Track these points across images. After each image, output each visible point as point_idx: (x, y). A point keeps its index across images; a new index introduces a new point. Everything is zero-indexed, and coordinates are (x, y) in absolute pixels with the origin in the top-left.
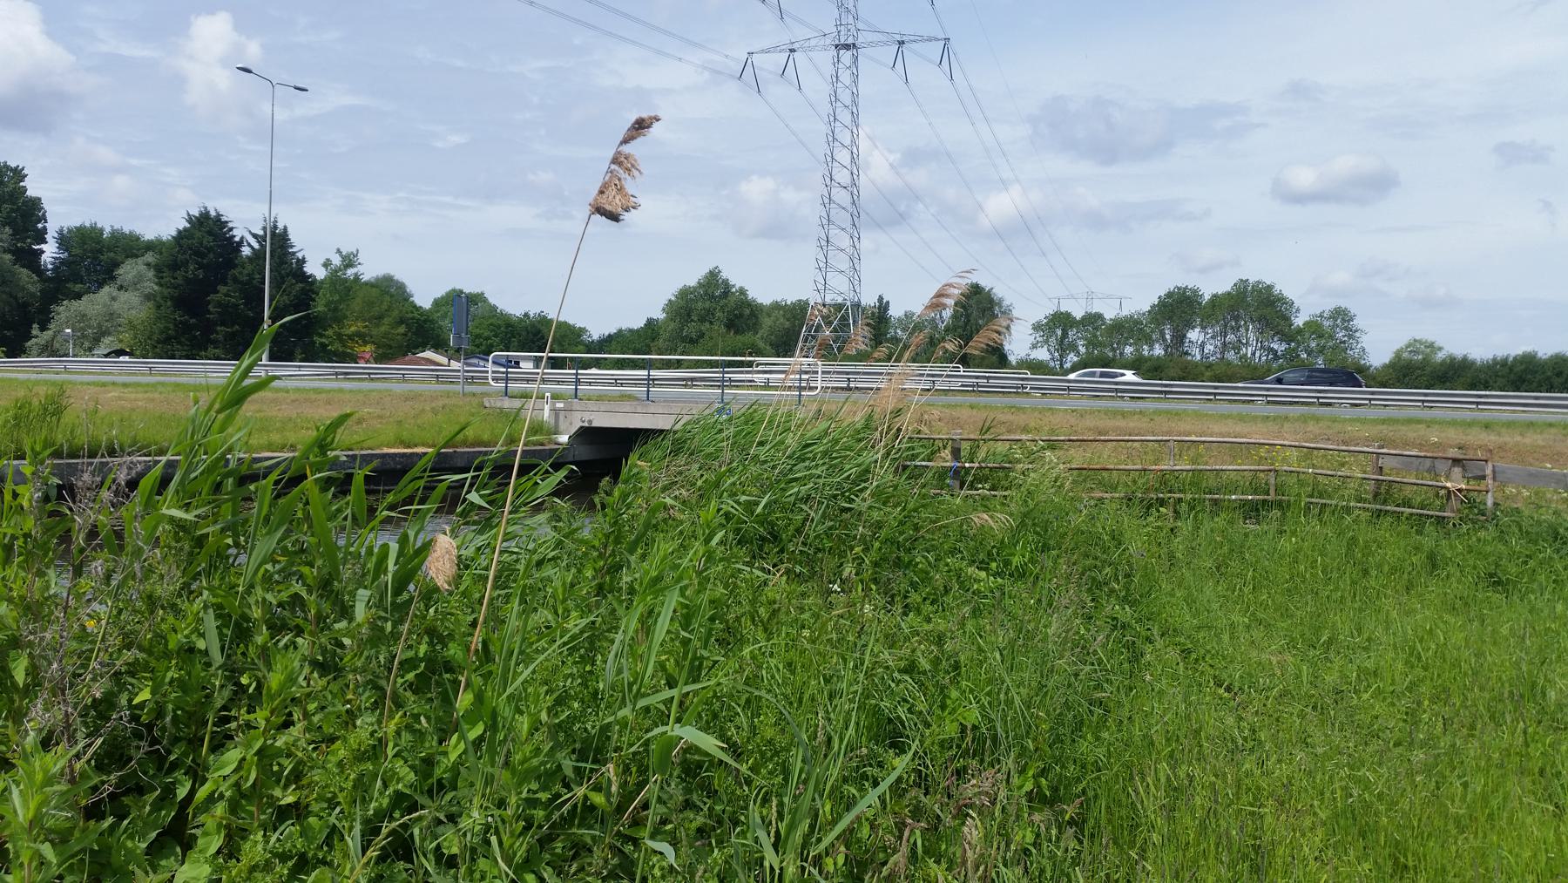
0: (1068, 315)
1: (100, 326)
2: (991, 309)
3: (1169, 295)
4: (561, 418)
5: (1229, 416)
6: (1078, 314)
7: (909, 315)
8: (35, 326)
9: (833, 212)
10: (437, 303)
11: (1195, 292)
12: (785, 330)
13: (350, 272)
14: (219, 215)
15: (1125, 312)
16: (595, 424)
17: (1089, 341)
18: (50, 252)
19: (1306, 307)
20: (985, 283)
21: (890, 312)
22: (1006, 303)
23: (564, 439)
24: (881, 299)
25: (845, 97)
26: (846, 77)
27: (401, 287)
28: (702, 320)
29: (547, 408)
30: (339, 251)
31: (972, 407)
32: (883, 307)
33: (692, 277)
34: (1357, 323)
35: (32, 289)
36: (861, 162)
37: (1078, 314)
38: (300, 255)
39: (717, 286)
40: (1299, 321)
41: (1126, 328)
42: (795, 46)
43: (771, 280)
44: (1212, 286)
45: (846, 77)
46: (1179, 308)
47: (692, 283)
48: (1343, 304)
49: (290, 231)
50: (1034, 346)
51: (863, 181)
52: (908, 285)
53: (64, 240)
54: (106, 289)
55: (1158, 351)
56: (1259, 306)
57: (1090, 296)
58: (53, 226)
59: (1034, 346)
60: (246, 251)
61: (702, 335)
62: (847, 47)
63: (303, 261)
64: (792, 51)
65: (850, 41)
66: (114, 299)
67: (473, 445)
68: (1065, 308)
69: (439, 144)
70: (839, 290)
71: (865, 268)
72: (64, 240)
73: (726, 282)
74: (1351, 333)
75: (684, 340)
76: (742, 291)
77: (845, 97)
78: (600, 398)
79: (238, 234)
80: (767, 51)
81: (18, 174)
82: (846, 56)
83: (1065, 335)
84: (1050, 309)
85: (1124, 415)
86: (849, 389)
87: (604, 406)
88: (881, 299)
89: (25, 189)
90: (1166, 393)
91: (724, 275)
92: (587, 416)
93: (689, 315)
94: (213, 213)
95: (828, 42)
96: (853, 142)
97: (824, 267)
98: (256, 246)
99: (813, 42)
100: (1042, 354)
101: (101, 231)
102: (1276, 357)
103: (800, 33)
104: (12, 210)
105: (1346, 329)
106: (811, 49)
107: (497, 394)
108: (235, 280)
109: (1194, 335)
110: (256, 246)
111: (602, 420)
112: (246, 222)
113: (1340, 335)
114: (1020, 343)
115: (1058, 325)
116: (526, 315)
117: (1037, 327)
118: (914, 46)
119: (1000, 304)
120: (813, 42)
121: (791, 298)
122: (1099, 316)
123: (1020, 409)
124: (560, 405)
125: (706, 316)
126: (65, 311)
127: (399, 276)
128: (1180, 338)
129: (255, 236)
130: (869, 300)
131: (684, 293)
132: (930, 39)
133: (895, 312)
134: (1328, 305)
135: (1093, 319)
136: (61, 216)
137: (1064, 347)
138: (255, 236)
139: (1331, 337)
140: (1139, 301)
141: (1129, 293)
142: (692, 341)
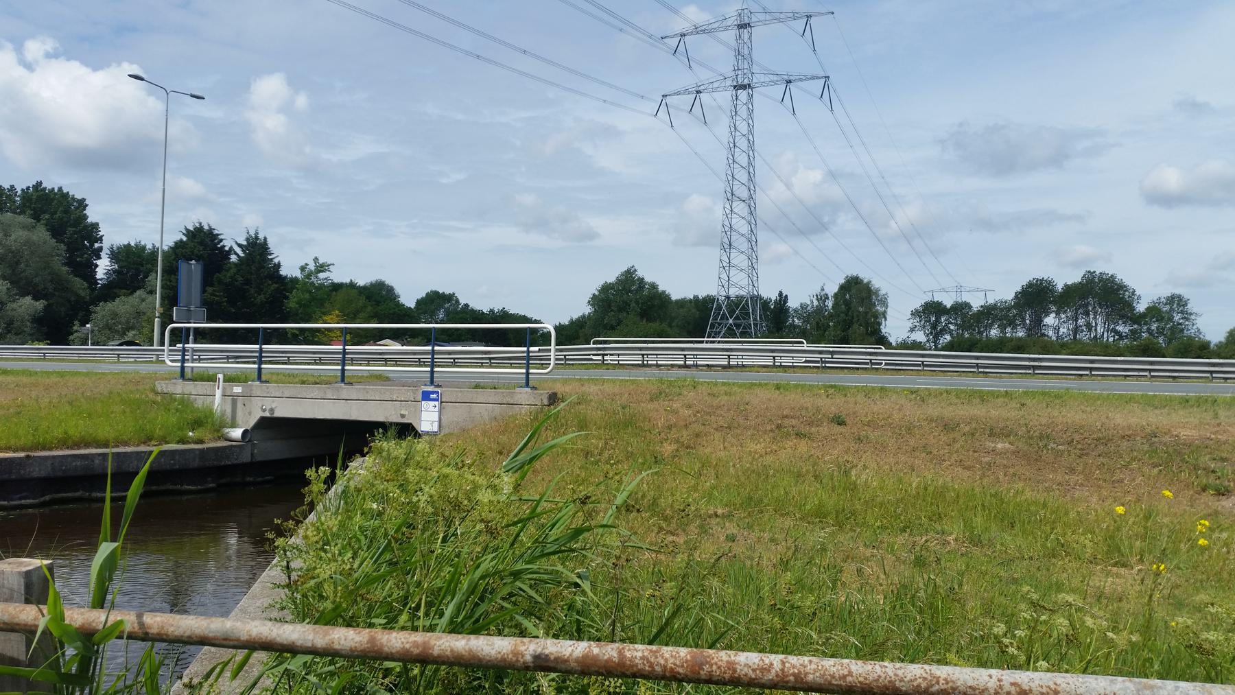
0: (940, 304)
1: (128, 322)
2: (869, 297)
3: (1030, 285)
4: (239, 405)
5: (1131, 400)
6: (948, 303)
7: (804, 306)
8: (77, 323)
9: (734, 221)
10: (419, 302)
11: (1050, 282)
12: (698, 319)
13: (321, 275)
14: (211, 230)
15: (991, 301)
16: (279, 413)
17: (960, 329)
18: (103, 266)
19: (1147, 290)
20: (865, 276)
21: (789, 304)
22: (882, 292)
23: (237, 433)
24: (781, 294)
25: (743, 127)
26: (743, 112)
27: (390, 290)
28: (620, 310)
29: (218, 393)
30: (316, 259)
31: (778, 387)
32: (782, 300)
33: (611, 276)
34: (1192, 307)
35: (82, 293)
36: (758, 179)
37: (948, 303)
38: (276, 261)
39: (633, 282)
40: (1141, 307)
41: (990, 313)
42: (701, 88)
43: (685, 278)
44: (1064, 277)
45: (743, 112)
46: (1037, 296)
47: (612, 279)
48: (1177, 291)
49: (269, 240)
50: (912, 330)
51: (760, 196)
52: (800, 276)
53: (115, 255)
54: (138, 293)
55: (1021, 333)
56: (1103, 294)
57: (959, 289)
58: (106, 244)
59: (912, 330)
60: (233, 258)
61: (619, 323)
62: (744, 87)
63: (279, 265)
64: (698, 92)
65: (746, 82)
66: (143, 300)
67: (77, 445)
68: (938, 298)
69: (444, 181)
70: (739, 287)
71: (762, 269)
72: (115, 255)
73: (641, 280)
74: (1187, 316)
75: (605, 327)
76: (654, 286)
77: (743, 127)
78: (290, 378)
79: (228, 244)
80: (678, 93)
81: (82, 204)
82: (743, 94)
83: (938, 321)
84: (927, 298)
85: (983, 397)
86: (686, 366)
87: (289, 390)
88: (781, 294)
89: (85, 217)
90: (1035, 368)
91: (640, 273)
92: (269, 403)
93: (609, 306)
94: (206, 227)
95: (729, 82)
96: (750, 163)
97: (727, 266)
98: (241, 254)
99: (716, 85)
100: (920, 337)
101: (144, 248)
102: (1121, 338)
103: (703, 76)
104: (75, 233)
105: (1182, 312)
106: (714, 90)
107: (169, 377)
108: (220, 282)
109: (1050, 320)
110: (241, 254)
111: (287, 409)
112: (232, 237)
113: (1177, 317)
114: (898, 324)
115: (931, 312)
116: (491, 311)
117: (915, 314)
118: (799, 83)
119: (876, 293)
120: (716, 85)
121: (702, 294)
122: (967, 305)
123: (843, 391)
124: (238, 389)
125: (624, 307)
126: (103, 310)
127: (388, 282)
128: (1037, 322)
129: (240, 245)
130: (769, 292)
131: (606, 288)
132: (813, 78)
133: (793, 304)
134: (1165, 292)
135: (960, 309)
136: (113, 236)
137: (936, 334)
138: (240, 245)
139: (1171, 319)
140: (1005, 292)
141: (996, 285)
142: (613, 328)
